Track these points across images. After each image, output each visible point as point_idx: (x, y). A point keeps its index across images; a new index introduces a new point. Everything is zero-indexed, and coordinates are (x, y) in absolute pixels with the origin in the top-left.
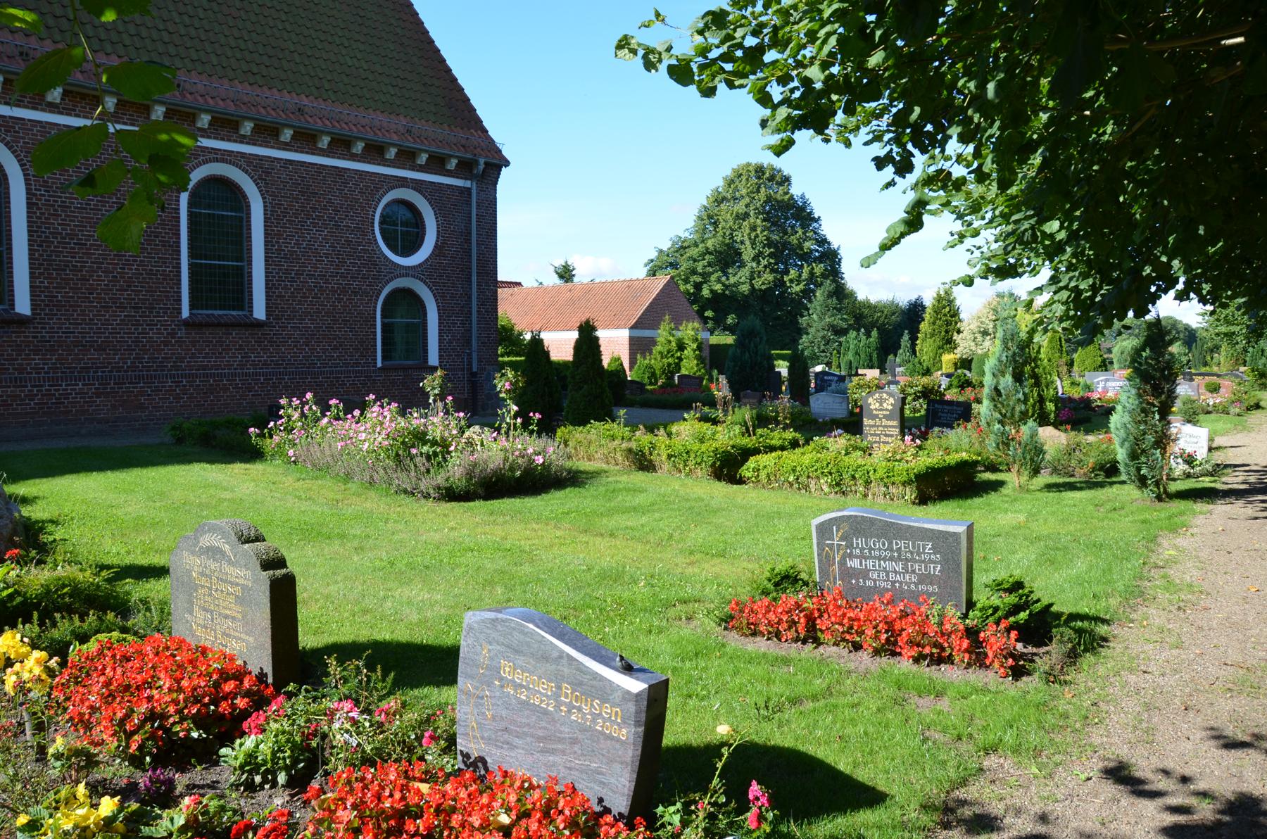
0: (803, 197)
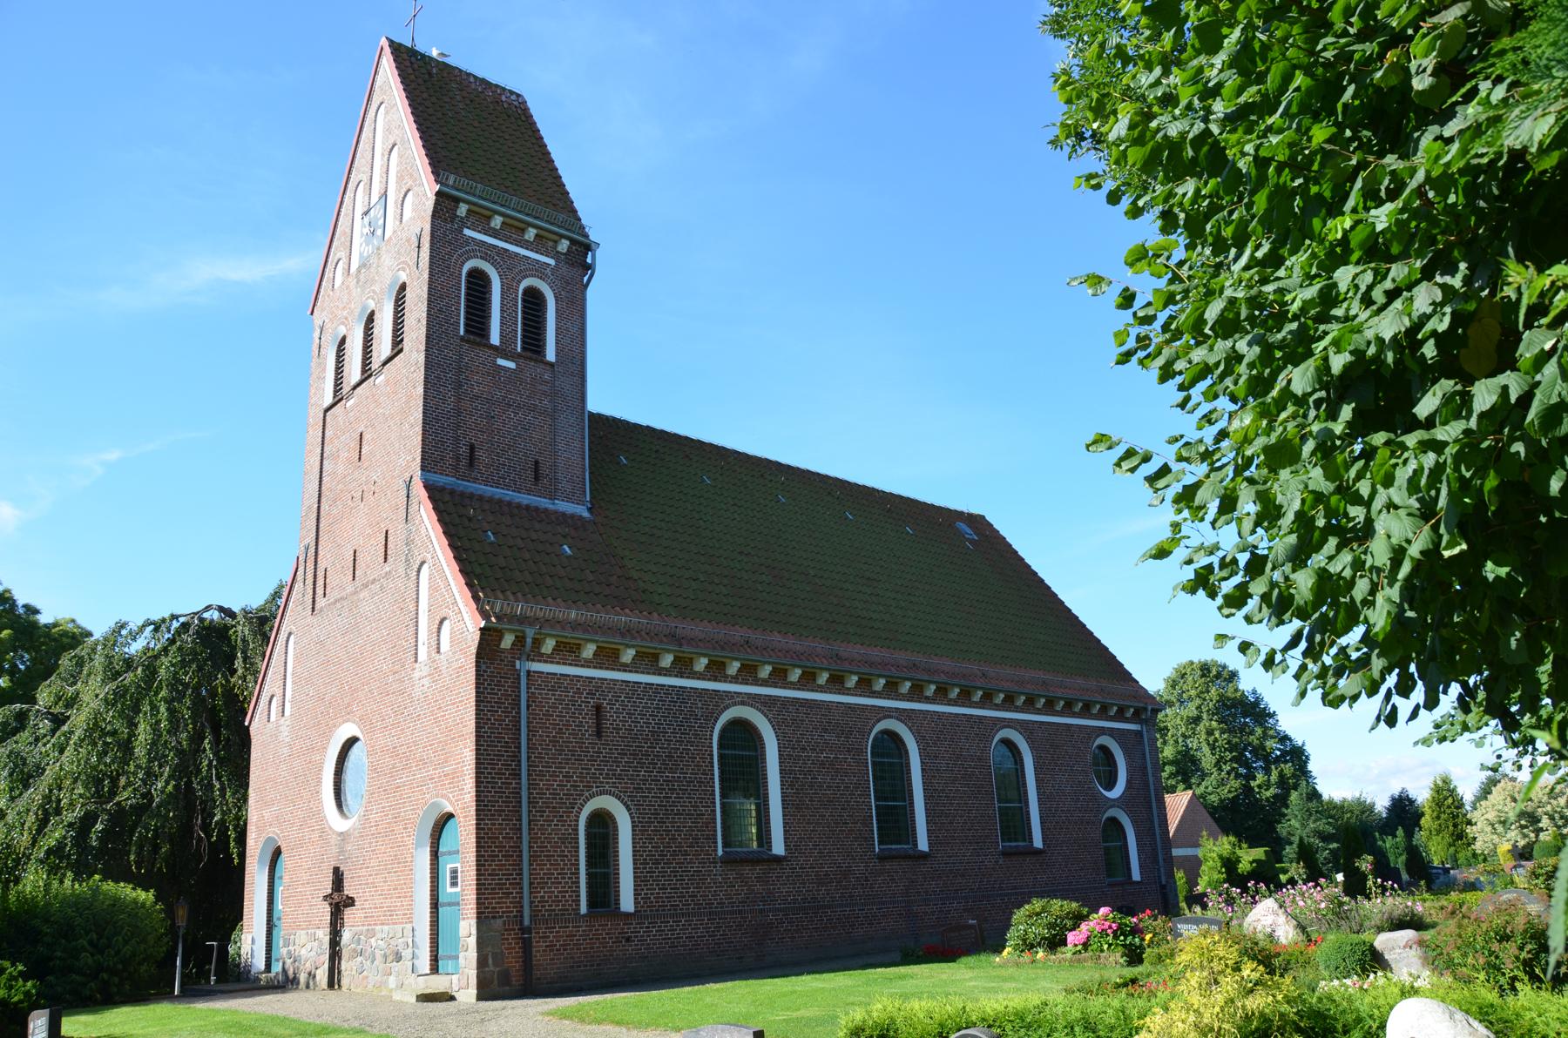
0: (1254, 692)
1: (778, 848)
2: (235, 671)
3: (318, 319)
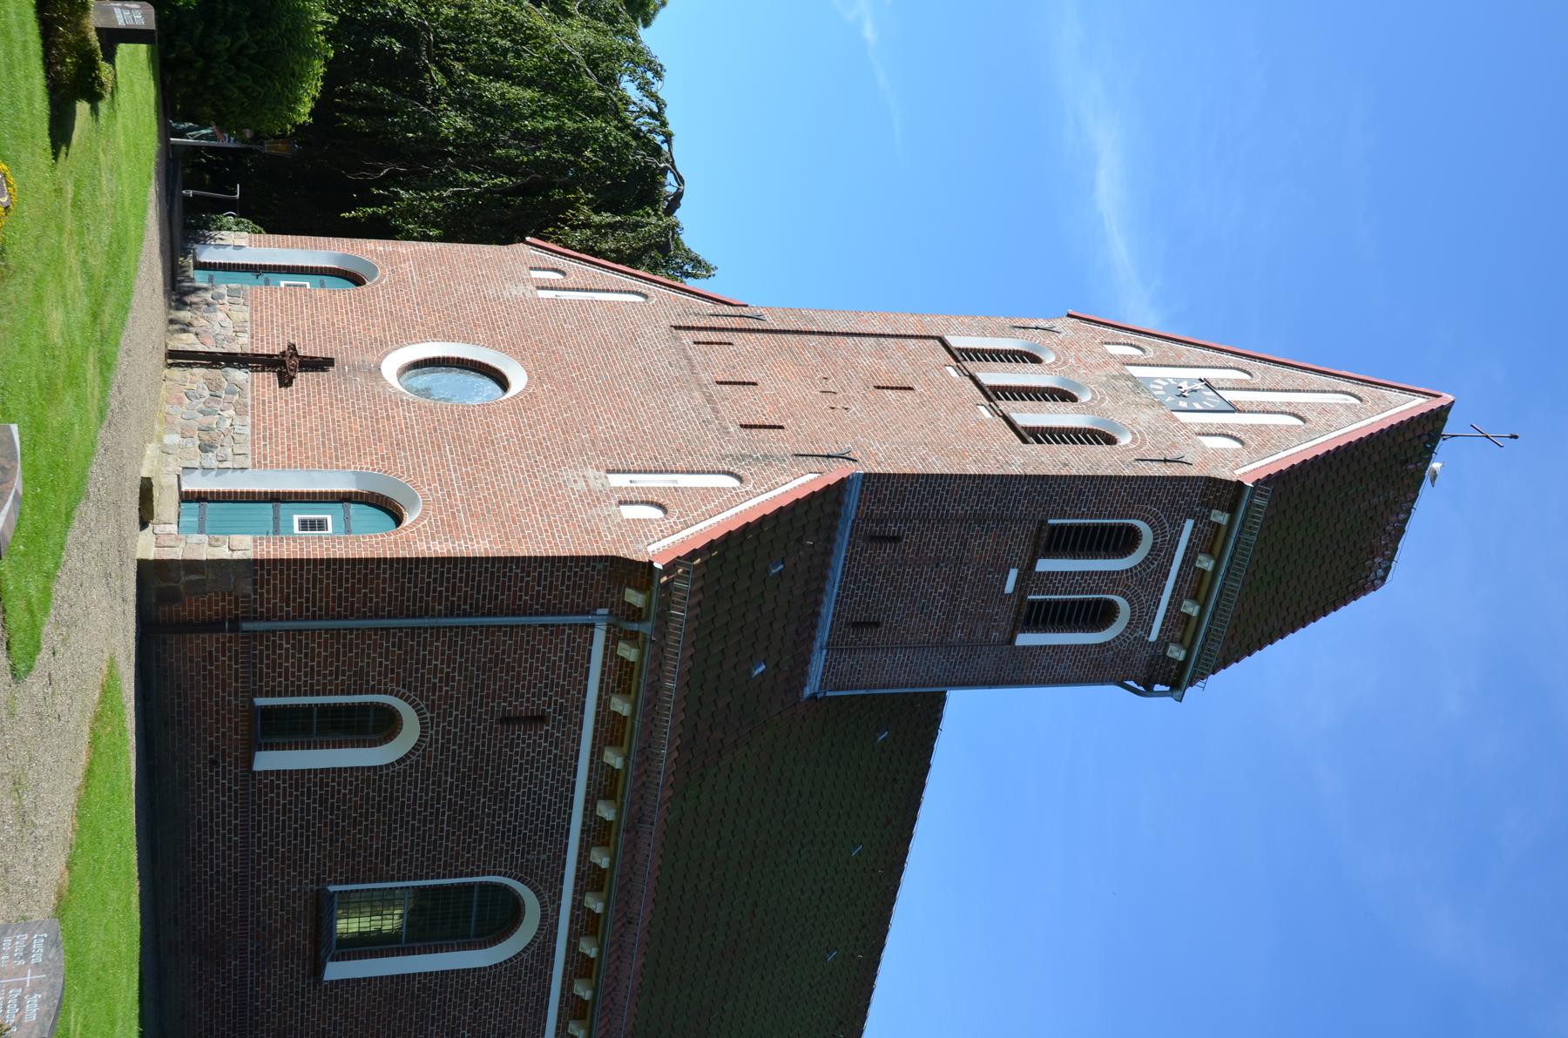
1: (336, 971)
2: (597, 212)
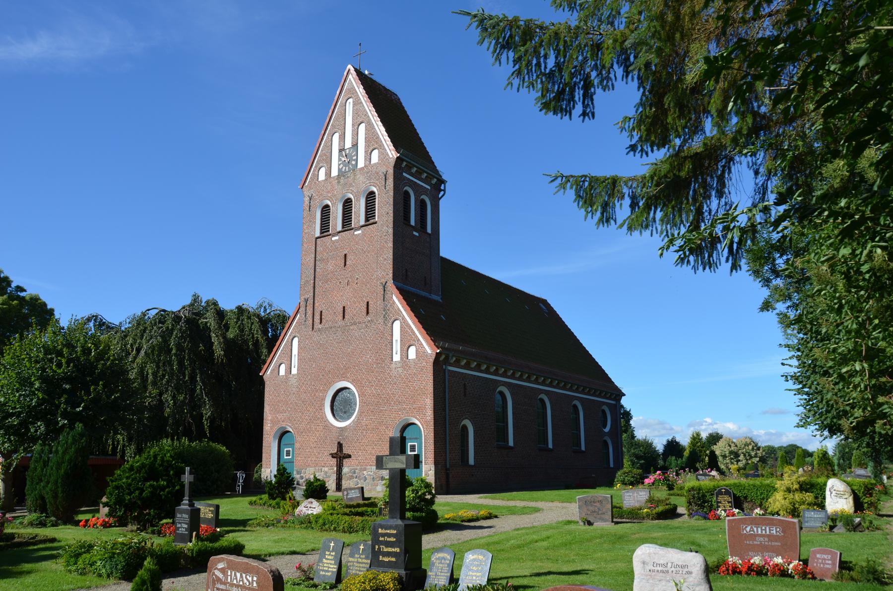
3: (307, 192)
